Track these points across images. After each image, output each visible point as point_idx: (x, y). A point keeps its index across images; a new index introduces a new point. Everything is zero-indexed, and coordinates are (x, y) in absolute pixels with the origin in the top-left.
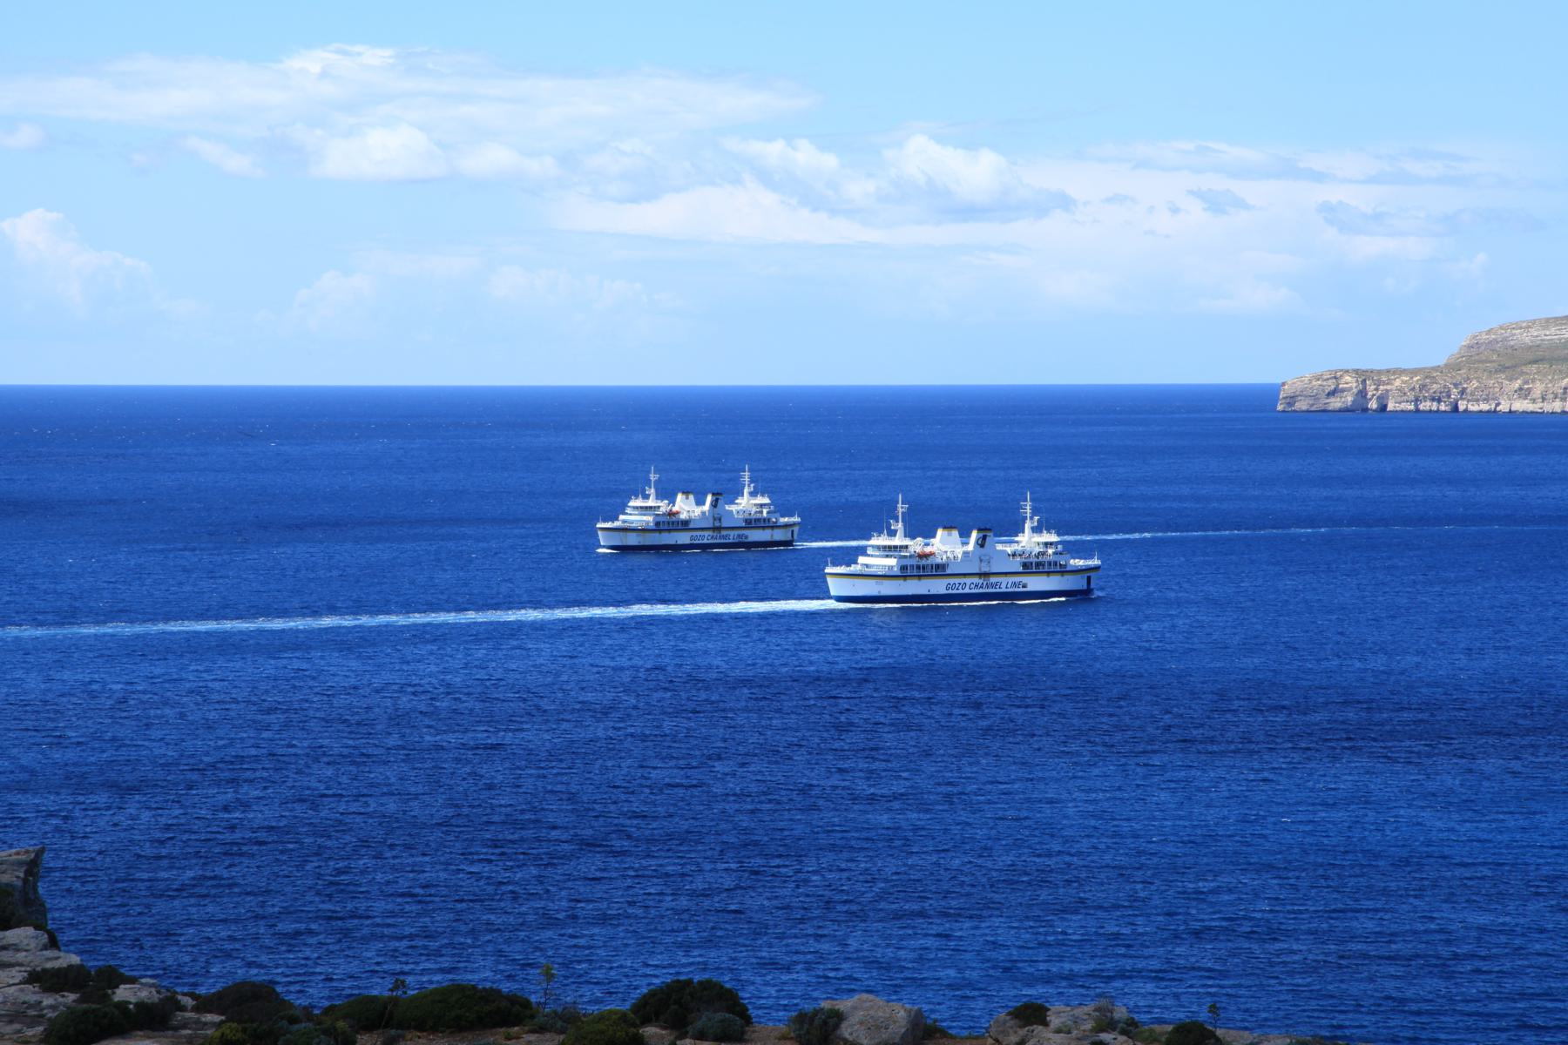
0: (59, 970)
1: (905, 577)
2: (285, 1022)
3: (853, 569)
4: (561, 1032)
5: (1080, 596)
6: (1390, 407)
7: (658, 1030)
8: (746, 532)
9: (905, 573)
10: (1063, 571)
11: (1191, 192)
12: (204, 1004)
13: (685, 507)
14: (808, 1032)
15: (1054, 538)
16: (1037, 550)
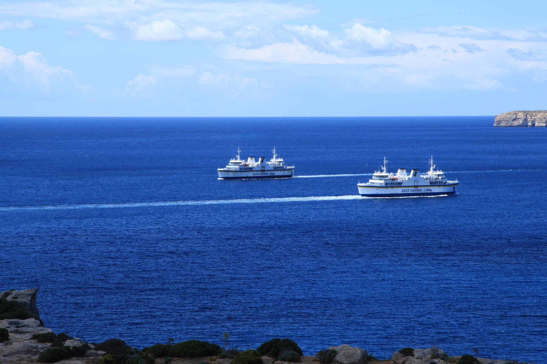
0: (44, 334)
1: (387, 187)
2: (128, 354)
3: (367, 184)
4: (231, 358)
5: (451, 194)
6: (536, 124)
7: (267, 358)
8: (274, 172)
9: (387, 186)
10: (445, 185)
11: (460, 45)
12: (98, 347)
13: (251, 162)
14: (324, 358)
15: (441, 173)
16: (435, 177)
